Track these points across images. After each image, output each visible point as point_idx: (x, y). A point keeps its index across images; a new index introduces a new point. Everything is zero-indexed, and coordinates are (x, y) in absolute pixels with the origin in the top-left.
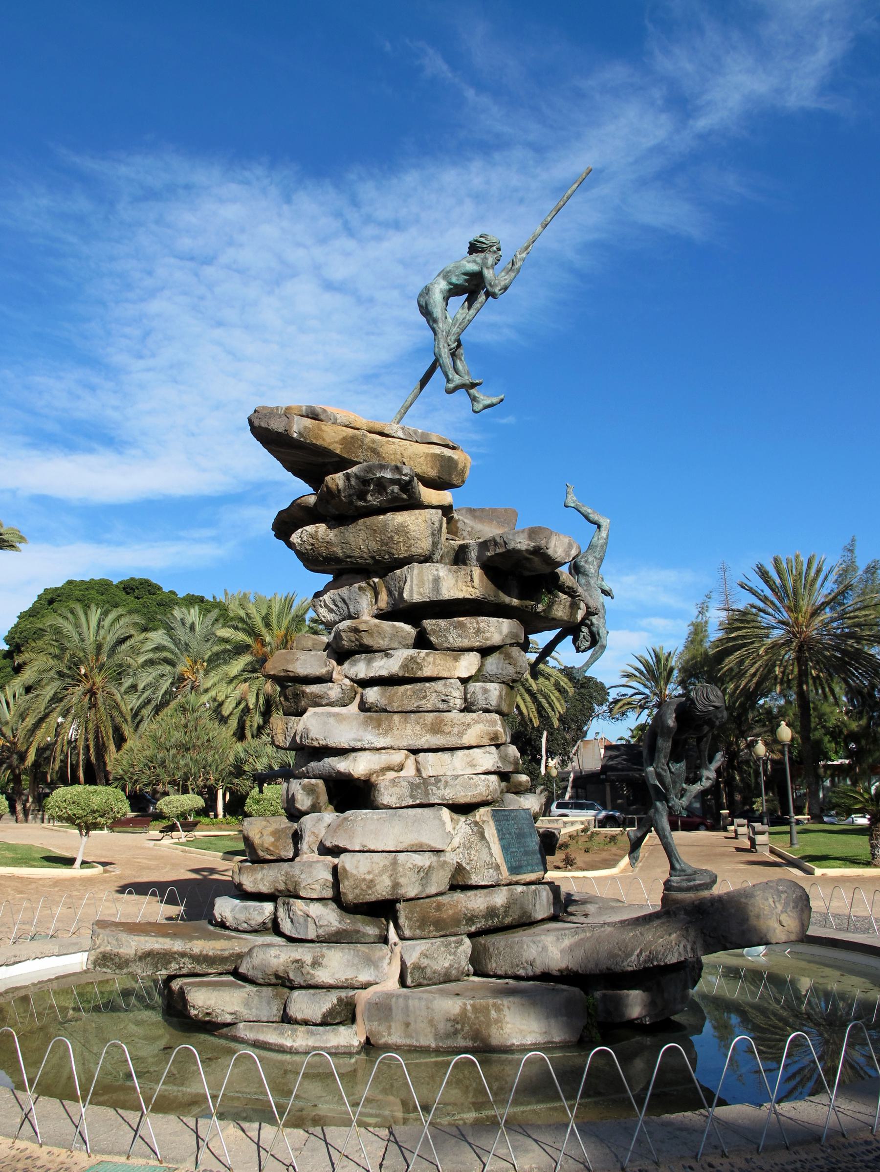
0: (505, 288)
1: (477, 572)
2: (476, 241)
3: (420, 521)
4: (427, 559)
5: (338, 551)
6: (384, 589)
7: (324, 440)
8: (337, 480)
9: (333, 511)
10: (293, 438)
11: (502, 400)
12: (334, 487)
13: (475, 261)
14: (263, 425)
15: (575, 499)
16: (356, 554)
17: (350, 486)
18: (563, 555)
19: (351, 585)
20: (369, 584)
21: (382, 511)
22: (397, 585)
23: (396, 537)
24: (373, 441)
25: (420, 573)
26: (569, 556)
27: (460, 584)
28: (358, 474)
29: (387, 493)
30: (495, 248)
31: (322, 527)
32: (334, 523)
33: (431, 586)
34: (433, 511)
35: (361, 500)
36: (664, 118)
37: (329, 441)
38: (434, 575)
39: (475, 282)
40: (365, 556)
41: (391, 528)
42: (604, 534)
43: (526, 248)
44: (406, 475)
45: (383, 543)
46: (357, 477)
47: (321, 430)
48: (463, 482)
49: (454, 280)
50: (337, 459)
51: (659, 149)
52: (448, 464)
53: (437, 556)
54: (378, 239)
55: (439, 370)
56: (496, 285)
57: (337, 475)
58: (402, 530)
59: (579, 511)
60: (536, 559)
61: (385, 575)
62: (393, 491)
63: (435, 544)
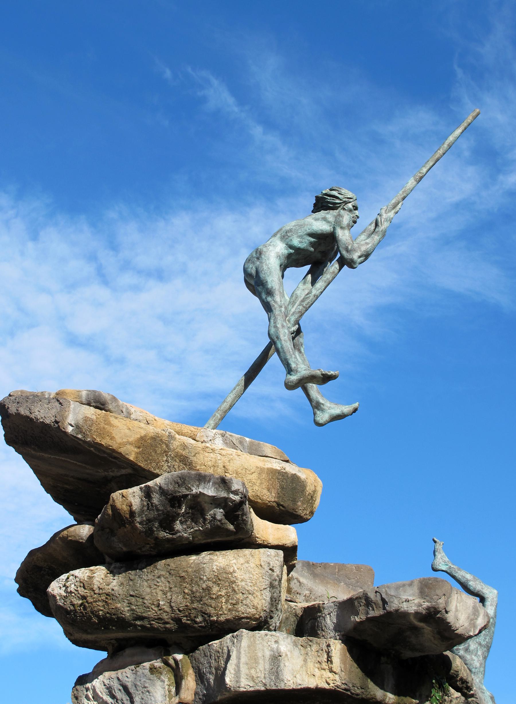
0: (366, 256)
1: (337, 648)
2: (326, 194)
3: (252, 565)
4: (260, 624)
5: (124, 609)
6: (191, 671)
7: (112, 438)
8: (130, 498)
9: (120, 547)
10: (65, 433)
11: (355, 410)
12: (125, 508)
13: (324, 219)
14: (23, 411)
15: (447, 559)
16: (151, 614)
17: (150, 506)
18: (466, 624)
19: (138, 664)
20: (166, 663)
21: (195, 549)
22: (214, 664)
23: (215, 589)
24: (184, 446)
25: (252, 646)
26: (474, 626)
27: (310, 665)
28: (165, 487)
29: (205, 520)
30: (350, 206)
31: (99, 572)
32: (118, 565)
33: (267, 666)
34: (272, 552)
35: (164, 529)
36: (471, 171)
37: (119, 440)
38: (272, 650)
39: (322, 248)
40: (165, 616)
41: (208, 574)
42: (491, 610)
43: (394, 207)
44: (236, 493)
45: (194, 597)
46: (162, 491)
47: (109, 424)
48: (312, 513)
49: (296, 242)
50: (129, 471)
51: (459, 207)
52: (292, 485)
53: (275, 621)
54: (136, 289)
55: (274, 359)
56: (354, 250)
57: (130, 490)
58: (223, 578)
59: (454, 577)
60: (427, 629)
61: (194, 649)
62: (214, 518)
63: (274, 601)
